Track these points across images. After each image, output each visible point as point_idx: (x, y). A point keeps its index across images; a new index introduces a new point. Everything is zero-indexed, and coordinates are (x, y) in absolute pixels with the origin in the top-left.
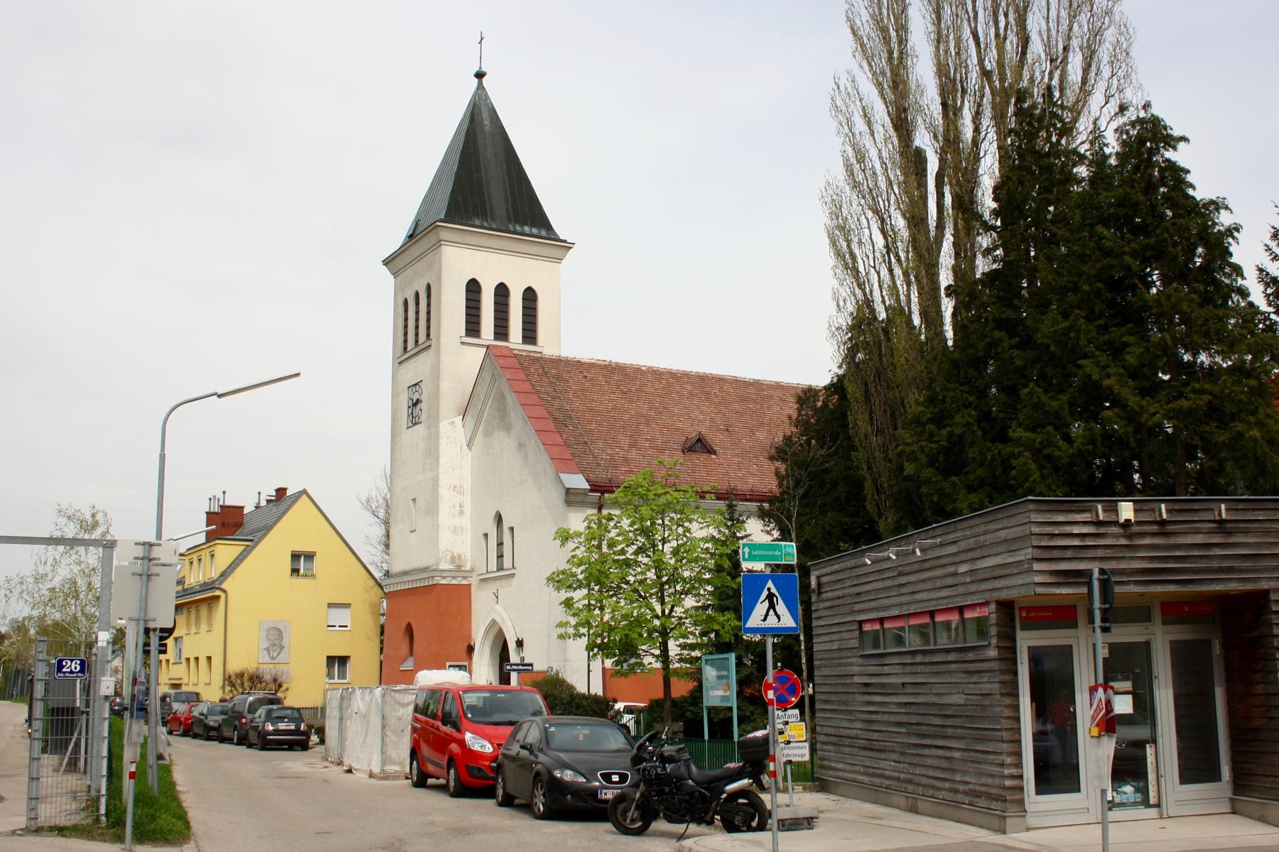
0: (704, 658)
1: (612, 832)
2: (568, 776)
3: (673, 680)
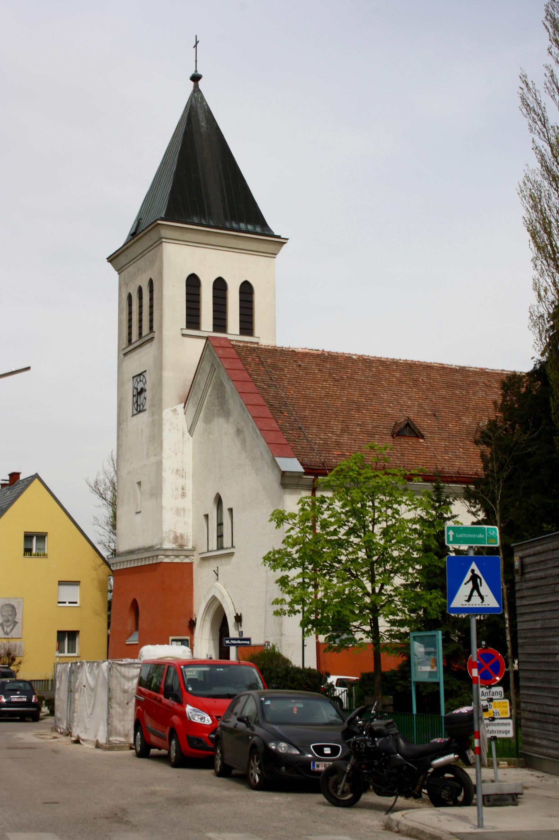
0: (412, 635)
1: (320, 803)
2: (283, 748)
3: (383, 655)
